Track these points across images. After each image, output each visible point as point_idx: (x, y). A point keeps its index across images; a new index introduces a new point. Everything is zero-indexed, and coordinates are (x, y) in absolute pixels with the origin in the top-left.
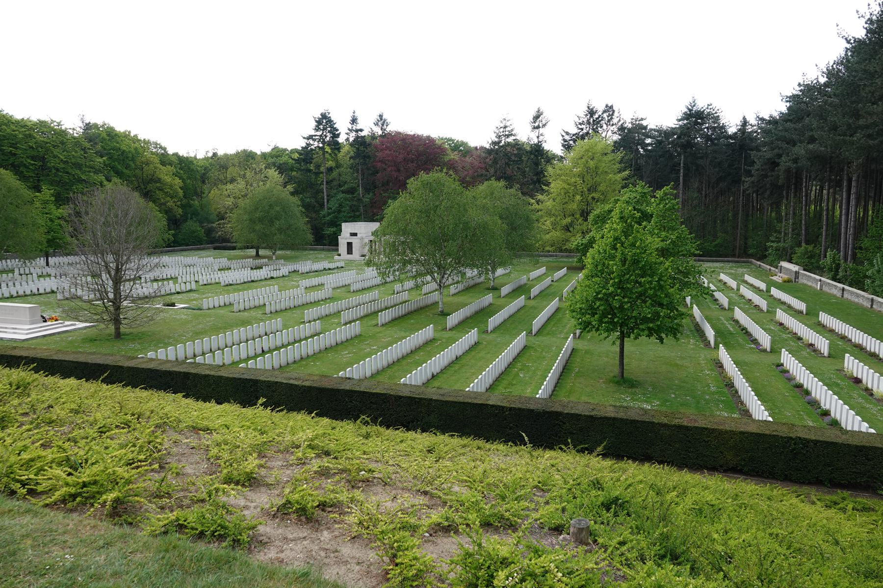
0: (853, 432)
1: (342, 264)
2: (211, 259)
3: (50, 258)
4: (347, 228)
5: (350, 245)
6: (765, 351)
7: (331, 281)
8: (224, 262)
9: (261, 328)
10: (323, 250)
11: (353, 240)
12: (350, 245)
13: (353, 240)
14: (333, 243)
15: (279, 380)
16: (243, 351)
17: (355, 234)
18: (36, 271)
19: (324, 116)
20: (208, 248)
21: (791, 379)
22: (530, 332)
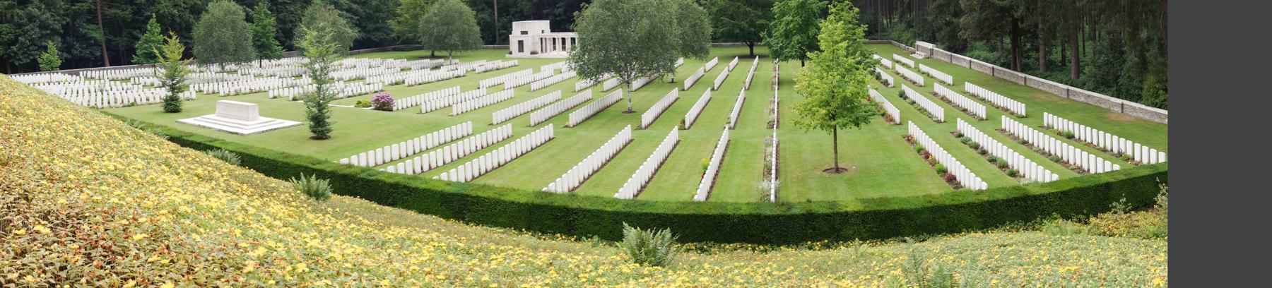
0: (1150, 166)
1: (516, 62)
4: (517, 26)
5: (521, 43)
6: (939, 122)
7: (510, 79)
8: (406, 63)
9: (456, 131)
11: (523, 38)
12: (521, 43)
13: (523, 38)
14: (506, 41)
16: (438, 157)
17: (526, 33)
18: (252, 71)
21: (934, 163)
22: (682, 128)
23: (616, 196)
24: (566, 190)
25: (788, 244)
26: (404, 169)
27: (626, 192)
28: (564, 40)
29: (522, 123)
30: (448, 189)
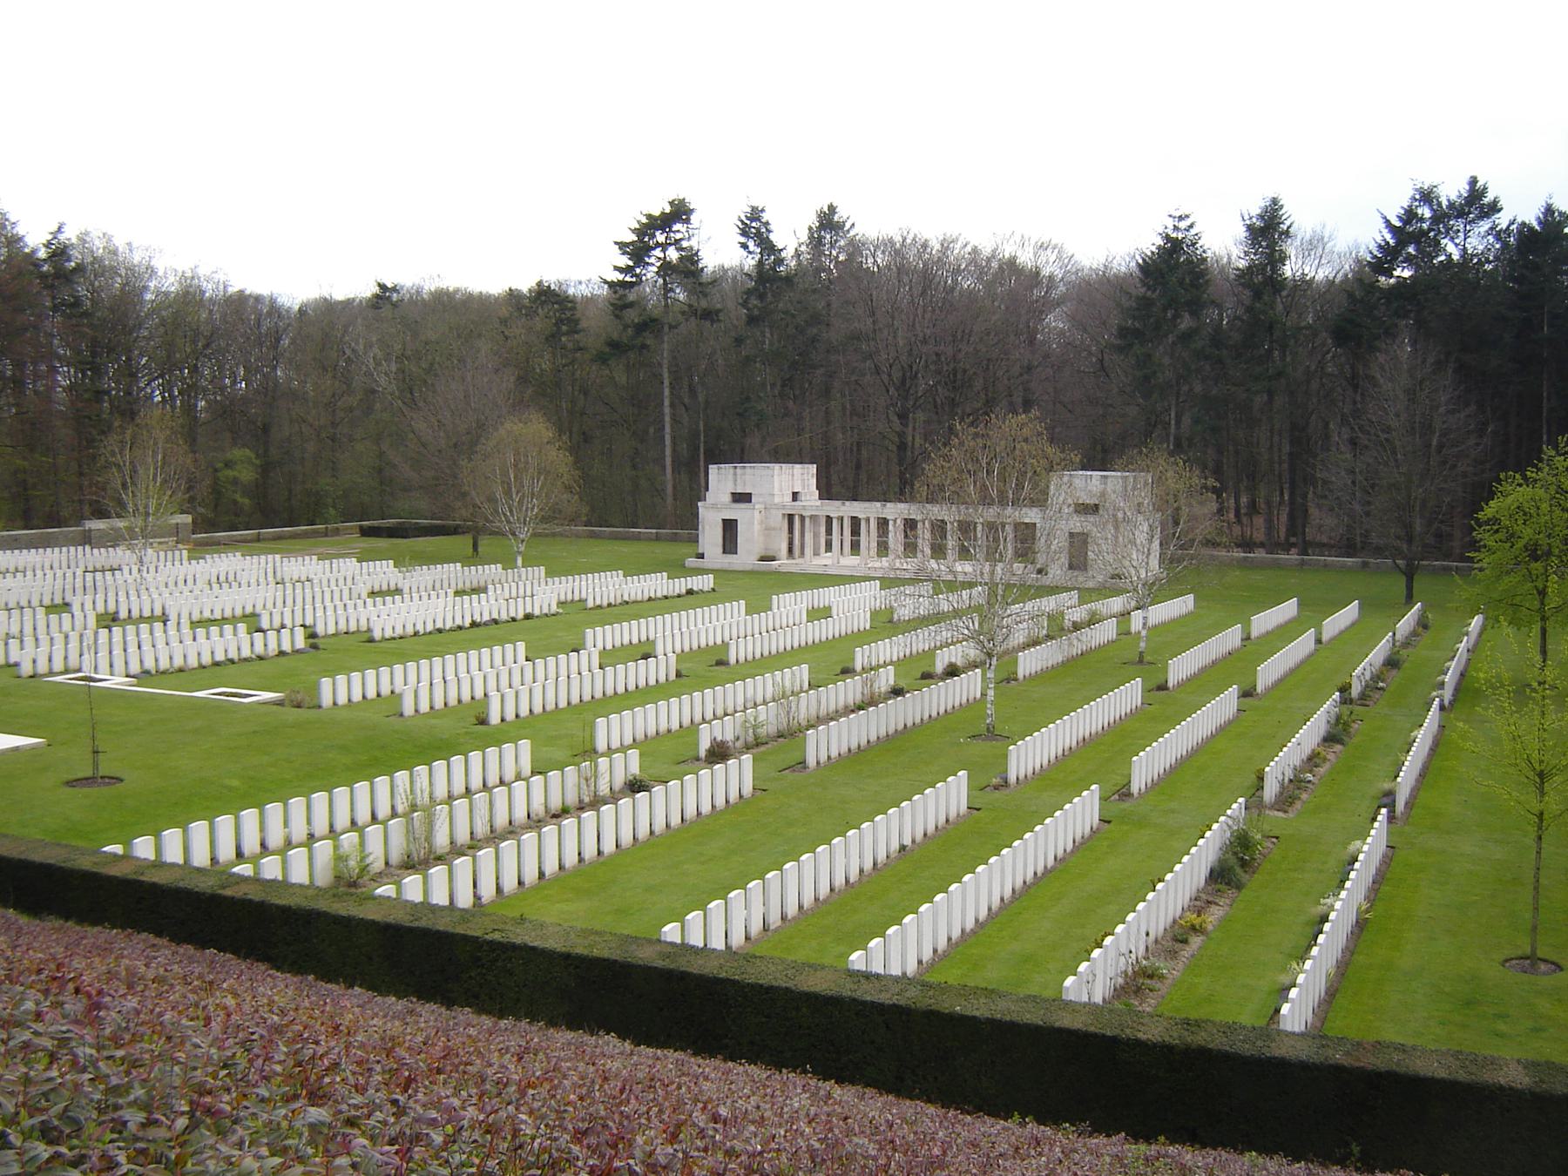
2: (351, 564)
3: (181, 862)
4: (722, 480)
5: (730, 527)
7: (678, 633)
10: (658, 538)
11: (736, 512)
12: (730, 527)
13: (736, 512)
14: (689, 522)
15: (563, 1036)
19: (755, 214)
20: (348, 531)
23: (856, 959)
24: (912, 968)
25: (236, 952)
26: (302, 871)
27: (1090, 982)
28: (883, 523)
29: (674, 755)
30: (868, 994)
